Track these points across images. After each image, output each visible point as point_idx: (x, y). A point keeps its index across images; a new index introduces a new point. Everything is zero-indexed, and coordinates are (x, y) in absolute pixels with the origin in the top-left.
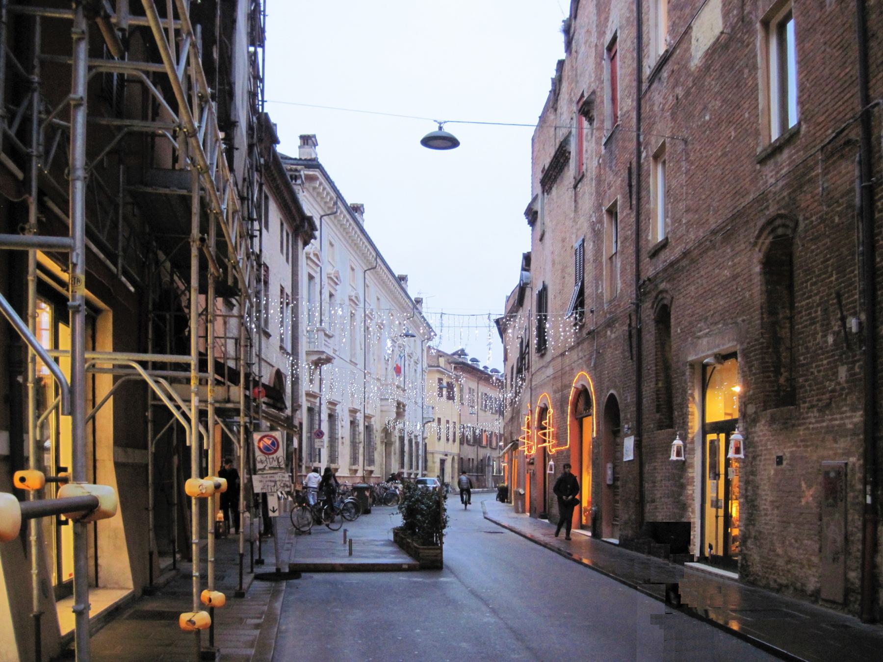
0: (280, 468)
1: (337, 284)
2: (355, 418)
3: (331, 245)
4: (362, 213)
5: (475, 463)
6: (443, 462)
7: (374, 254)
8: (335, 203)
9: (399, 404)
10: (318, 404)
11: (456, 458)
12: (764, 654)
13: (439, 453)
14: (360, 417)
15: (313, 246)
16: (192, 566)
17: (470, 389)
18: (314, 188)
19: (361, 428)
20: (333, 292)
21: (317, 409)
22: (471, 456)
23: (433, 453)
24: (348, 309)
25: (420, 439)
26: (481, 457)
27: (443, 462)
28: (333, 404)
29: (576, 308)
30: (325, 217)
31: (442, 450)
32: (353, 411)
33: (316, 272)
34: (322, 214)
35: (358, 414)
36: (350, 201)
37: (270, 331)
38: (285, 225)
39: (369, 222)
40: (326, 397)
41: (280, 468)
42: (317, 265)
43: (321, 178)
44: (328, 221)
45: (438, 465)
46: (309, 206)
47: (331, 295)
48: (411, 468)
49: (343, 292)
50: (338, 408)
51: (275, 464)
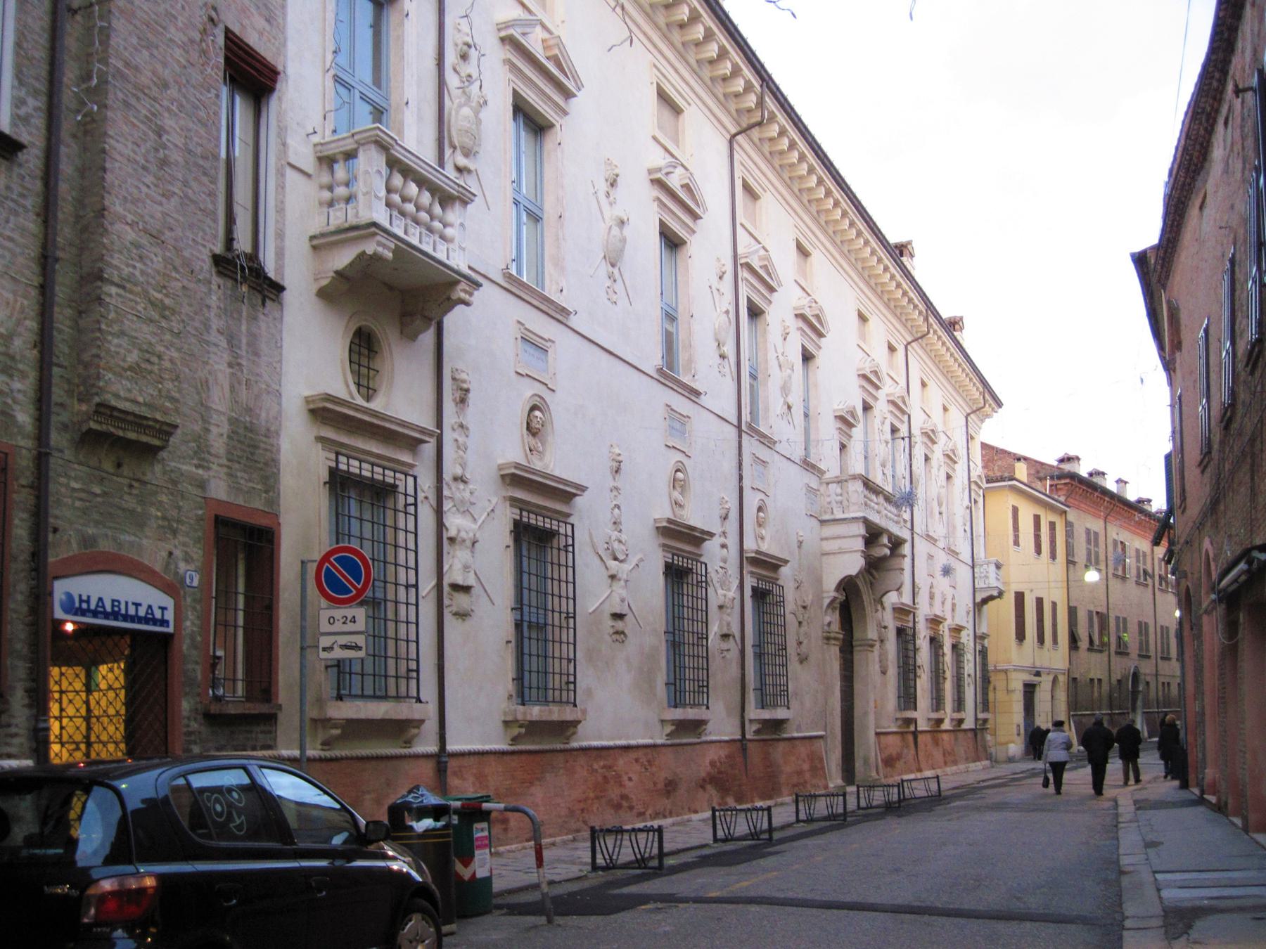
1: (877, 388)
2: (936, 631)
3: (924, 385)
4: (961, 329)
5: (1105, 687)
6: (1030, 689)
7: (922, 307)
8: (761, 103)
9: (873, 535)
10: (911, 625)
11: (1062, 679)
13: (1018, 669)
14: (944, 629)
17: (1088, 531)
19: (947, 649)
20: (951, 473)
21: (910, 632)
22: (1096, 674)
23: (1006, 671)
25: (967, 638)
26: (1117, 676)
27: (1030, 689)
30: (739, 137)
31: (1027, 662)
33: (902, 422)
34: (733, 131)
35: (964, 633)
36: (946, 314)
39: (919, 267)
42: (903, 412)
44: (920, 352)
45: (1018, 697)
47: (927, 459)
48: (938, 703)
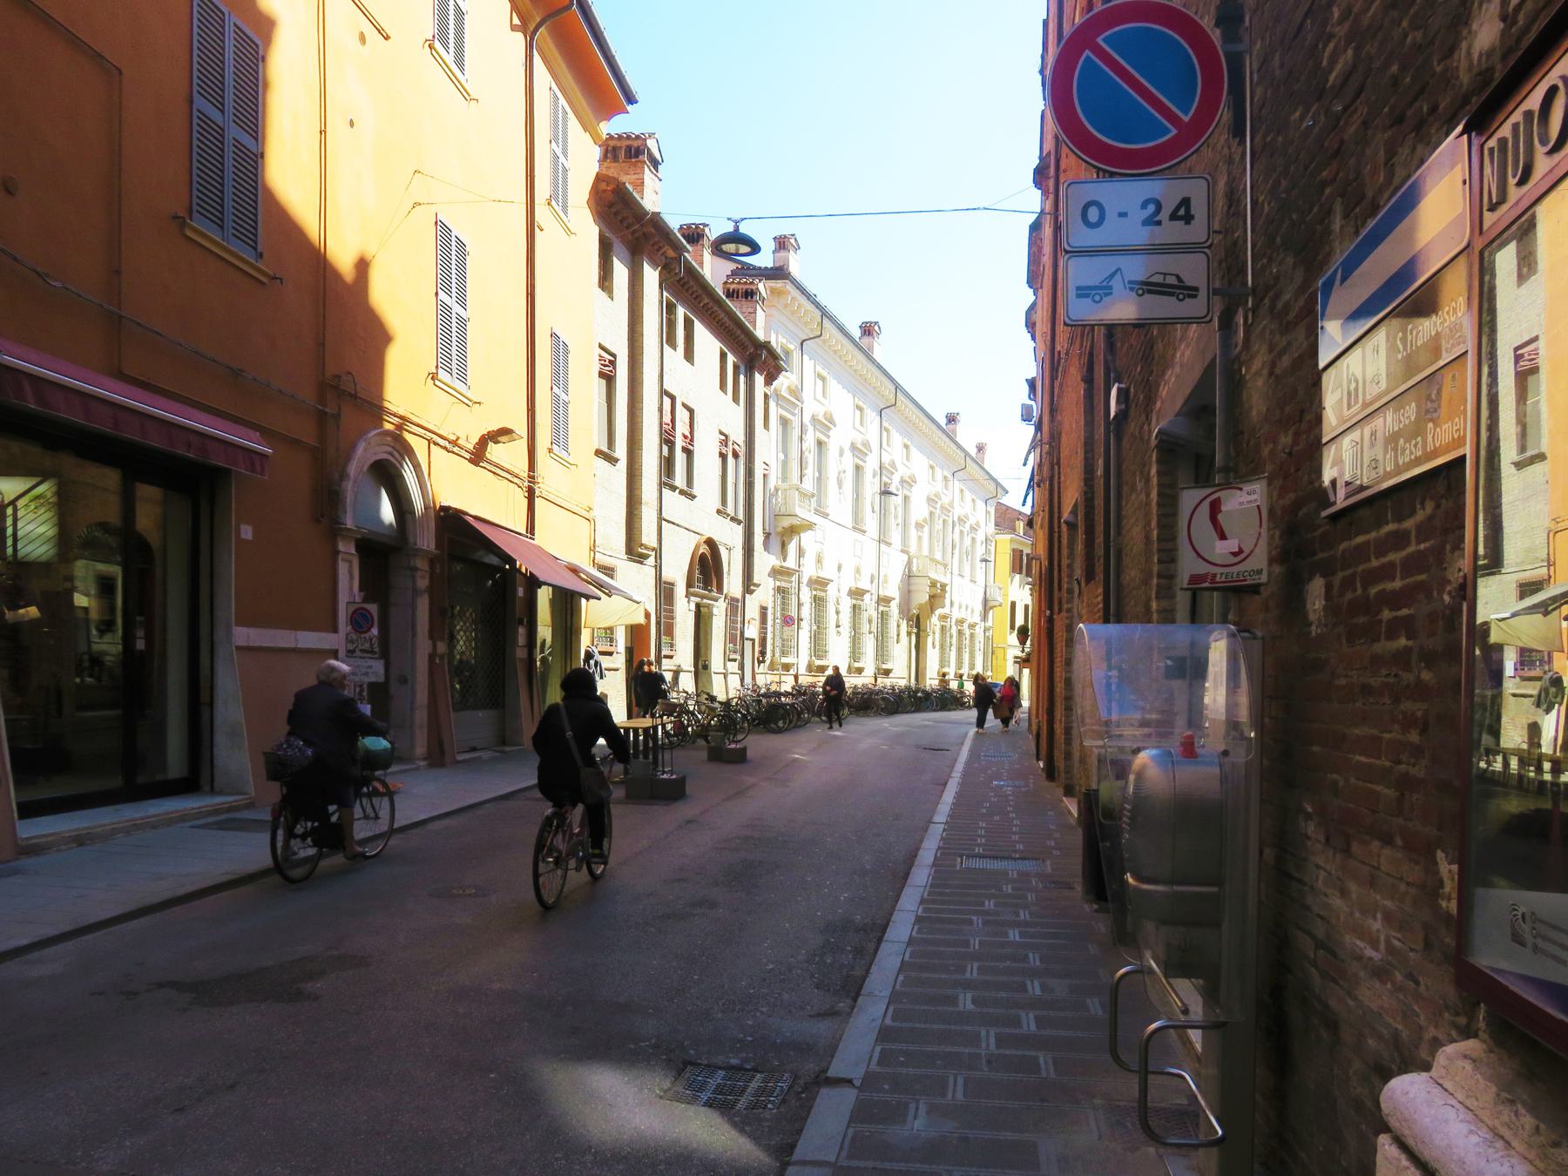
0: (372, 652)
12: (811, 289)
15: (783, 382)
16: (17, 797)
18: (786, 306)
24: (849, 461)
28: (820, 584)
29: (1535, 370)
32: (857, 593)
35: (867, 597)
37: (695, 492)
38: (731, 359)
40: (809, 570)
41: (372, 652)
43: (795, 293)
46: (763, 325)
47: (820, 443)
49: (838, 439)
50: (831, 590)
51: (367, 646)
